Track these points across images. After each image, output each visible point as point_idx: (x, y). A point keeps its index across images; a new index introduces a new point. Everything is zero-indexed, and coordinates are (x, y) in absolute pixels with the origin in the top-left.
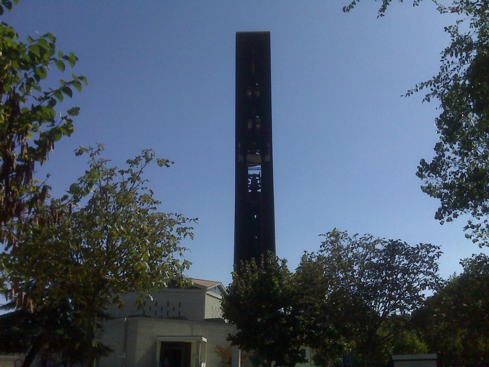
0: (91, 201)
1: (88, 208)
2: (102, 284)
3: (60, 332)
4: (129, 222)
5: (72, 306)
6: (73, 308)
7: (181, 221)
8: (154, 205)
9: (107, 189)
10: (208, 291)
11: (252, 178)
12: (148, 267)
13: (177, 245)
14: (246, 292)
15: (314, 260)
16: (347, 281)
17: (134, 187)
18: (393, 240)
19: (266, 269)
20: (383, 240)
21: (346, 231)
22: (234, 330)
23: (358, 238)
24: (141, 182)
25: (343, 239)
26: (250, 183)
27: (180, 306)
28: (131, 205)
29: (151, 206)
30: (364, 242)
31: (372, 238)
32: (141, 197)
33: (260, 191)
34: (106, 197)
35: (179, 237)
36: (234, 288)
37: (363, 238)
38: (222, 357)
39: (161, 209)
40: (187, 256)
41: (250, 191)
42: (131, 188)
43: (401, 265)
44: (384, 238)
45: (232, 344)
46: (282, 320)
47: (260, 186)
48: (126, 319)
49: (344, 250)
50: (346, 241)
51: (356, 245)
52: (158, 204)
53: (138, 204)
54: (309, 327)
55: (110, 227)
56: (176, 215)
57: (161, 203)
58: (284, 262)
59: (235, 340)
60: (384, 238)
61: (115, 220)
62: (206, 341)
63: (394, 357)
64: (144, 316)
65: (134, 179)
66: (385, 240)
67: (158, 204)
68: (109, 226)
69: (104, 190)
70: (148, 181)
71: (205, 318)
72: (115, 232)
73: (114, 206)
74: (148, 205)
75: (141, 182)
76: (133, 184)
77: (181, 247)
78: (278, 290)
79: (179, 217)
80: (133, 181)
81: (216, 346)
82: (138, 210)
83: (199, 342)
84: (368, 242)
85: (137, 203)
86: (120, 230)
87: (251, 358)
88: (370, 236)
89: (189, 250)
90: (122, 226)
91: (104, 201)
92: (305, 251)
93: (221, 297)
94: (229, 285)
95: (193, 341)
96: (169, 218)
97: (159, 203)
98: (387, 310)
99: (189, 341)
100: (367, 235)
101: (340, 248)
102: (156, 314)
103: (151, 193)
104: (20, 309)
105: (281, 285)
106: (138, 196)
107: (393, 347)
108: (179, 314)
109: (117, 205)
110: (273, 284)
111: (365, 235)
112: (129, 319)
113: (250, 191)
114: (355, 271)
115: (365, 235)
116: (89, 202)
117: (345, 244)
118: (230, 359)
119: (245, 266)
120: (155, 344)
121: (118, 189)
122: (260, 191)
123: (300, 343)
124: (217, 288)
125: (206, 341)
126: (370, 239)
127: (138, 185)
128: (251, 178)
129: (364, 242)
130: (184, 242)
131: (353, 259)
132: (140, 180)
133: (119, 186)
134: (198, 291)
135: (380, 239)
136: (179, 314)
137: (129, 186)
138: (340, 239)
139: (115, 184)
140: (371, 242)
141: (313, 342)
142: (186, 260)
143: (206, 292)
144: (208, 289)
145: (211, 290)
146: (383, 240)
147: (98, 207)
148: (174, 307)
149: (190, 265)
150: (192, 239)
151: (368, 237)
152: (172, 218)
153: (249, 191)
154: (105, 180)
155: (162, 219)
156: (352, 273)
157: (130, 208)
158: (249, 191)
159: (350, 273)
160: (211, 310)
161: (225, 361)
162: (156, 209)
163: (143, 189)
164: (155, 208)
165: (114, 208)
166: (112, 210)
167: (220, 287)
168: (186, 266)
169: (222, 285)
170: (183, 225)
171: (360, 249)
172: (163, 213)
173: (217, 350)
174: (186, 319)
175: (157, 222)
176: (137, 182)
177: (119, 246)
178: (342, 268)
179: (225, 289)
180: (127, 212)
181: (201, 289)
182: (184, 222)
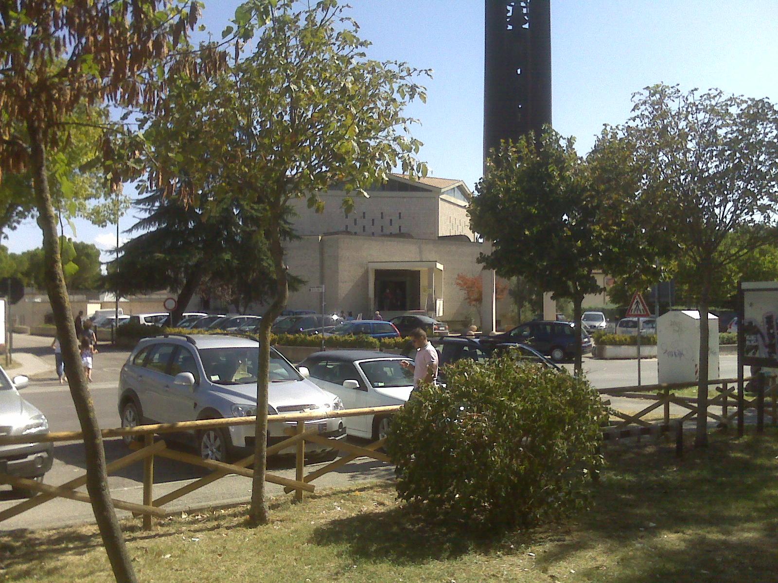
0: (260, 44)
1: (258, 55)
2: (283, 184)
3: (227, 256)
4: (323, 76)
5: (239, 219)
6: (241, 223)
7: (404, 74)
8: (361, 49)
9: (285, 23)
10: (443, 193)
11: (513, 4)
12: (357, 149)
13: (400, 115)
14: (507, 190)
15: (620, 135)
16: (674, 167)
17: (326, 18)
18: (754, 99)
19: (539, 154)
20: (741, 98)
21: (678, 85)
22: (489, 249)
23: (697, 95)
24: (339, 9)
25: (672, 98)
26: (509, 14)
27: (400, 217)
28: (324, 48)
29: (356, 51)
30: (708, 102)
31: (722, 95)
32: (339, 34)
33: (528, 27)
34: (284, 36)
35: (403, 101)
36: (486, 186)
37: (705, 97)
38: (466, 292)
39: (373, 54)
40: (414, 132)
41: (510, 27)
42: (322, 21)
43: (766, 139)
44: (742, 96)
45: (484, 268)
46: (564, 232)
47: (527, 19)
48: (320, 238)
49: (673, 117)
50: (677, 100)
51: (694, 108)
52: (367, 47)
53: (335, 48)
54: (607, 241)
55: (295, 87)
56: (396, 64)
57: (371, 43)
58: (571, 141)
59: (489, 262)
60: (742, 96)
61: (300, 75)
62: (442, 269)
63: (745, 285)
64: (347, 232)
65: (326, 4)
66: (744, 98)
67: (367, 47)
68: (293, 87)
69: (281, 24)
70: (350, 7)
71: (440, 235)
72: (302, 95)
73: (297, 53)
74: (351, 48)
75: (339, 9)
76: (325, 13)
77: (406, 117)
78: (558, 186)
79: (402, 67)
80: (326, 9)
81: (458, 275)
82: (336, 58)
83: (432, 270)
84: (713, 103)
85: (333, 45)
86: (311, 92)
87: (512, 293)
88: (719, 91)
89: (418, 121)
90: (312, 86)
91: (280, 44)
92: (604, 125)
93: (465, 203)
94: (480, 179)
95: (423, 269)
96: (386, 69)
97: (368, 44)
98: (738, 212)
99: (417, 269)
100: (712, 90)
101: (664, 115)
102: (364, 230)
103: (354, 28)
104: (163, 226)
105: (563, 178)
106: (335, 35)
107: (741, 275)
108: (400, 230)
109: (302, 50)
110: (550, 177)
111: (710, 90)
112: (326, 238)
113: (510, 27)
114: (689, 150)
115: (710, 90)
116: (259, 46)
117: (674, 106)
118: (481, 294)
119: (506, 150)
120: (367, 272)
121: (302, 23)
122: (526, 26)
123: (591, 265)
124: (456, 189)
125: (442, 269)
126: (718, 97)
127: (334, 14)
128: (512, 6)
129: (708, 102)
130: (410, 109)
131: (686, 130)
132: (337, 6)
133: (303, 17)
134: (425, 194)
135: (735, 97)
136: (400, 230)
137: (319, 16)
138: (667, 98)
139: (296, 14)
140: (719, 102)
141: (612, 264)
142: (414, 139)
143: (440, 197)
144: (443, 190)
145: (446, 192)
146: (741, 98)
147: (273, 54)
148: (391, 220)
149: (420, 147)
150: (425, 102)
151: (716, 93)
152: (390, 69)
153: (508, 28)
154: (279, 9)
155: (374, 70)
156: (684, 154)
157: (322, 54)
158: (508, 28)
159: (680, 156)
160: (448, 223)
161: (472, 297)
162: (365, 56)
163: (342, 20)
164: (363, 55)
165: (297, 55)
166: (295, 58)
167: (461, 189)
168: (414, 147)
169: (464, 185)
170: (409, 81)
171: (701, 116)
172: (375, 62)
173: (460, 282)
174: (411, 237)
175: (368, 77)
176: (331, 10)
177: (310, 116)
178: (667, 146)
179: (471, 188)
180: (319, 62)
181: (431, 191)
182: (409, 74)
